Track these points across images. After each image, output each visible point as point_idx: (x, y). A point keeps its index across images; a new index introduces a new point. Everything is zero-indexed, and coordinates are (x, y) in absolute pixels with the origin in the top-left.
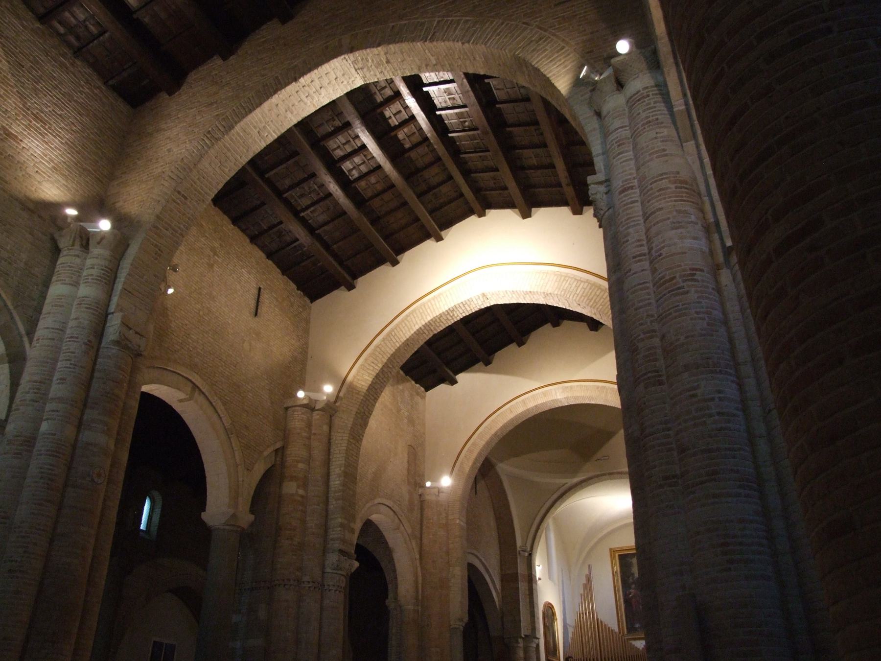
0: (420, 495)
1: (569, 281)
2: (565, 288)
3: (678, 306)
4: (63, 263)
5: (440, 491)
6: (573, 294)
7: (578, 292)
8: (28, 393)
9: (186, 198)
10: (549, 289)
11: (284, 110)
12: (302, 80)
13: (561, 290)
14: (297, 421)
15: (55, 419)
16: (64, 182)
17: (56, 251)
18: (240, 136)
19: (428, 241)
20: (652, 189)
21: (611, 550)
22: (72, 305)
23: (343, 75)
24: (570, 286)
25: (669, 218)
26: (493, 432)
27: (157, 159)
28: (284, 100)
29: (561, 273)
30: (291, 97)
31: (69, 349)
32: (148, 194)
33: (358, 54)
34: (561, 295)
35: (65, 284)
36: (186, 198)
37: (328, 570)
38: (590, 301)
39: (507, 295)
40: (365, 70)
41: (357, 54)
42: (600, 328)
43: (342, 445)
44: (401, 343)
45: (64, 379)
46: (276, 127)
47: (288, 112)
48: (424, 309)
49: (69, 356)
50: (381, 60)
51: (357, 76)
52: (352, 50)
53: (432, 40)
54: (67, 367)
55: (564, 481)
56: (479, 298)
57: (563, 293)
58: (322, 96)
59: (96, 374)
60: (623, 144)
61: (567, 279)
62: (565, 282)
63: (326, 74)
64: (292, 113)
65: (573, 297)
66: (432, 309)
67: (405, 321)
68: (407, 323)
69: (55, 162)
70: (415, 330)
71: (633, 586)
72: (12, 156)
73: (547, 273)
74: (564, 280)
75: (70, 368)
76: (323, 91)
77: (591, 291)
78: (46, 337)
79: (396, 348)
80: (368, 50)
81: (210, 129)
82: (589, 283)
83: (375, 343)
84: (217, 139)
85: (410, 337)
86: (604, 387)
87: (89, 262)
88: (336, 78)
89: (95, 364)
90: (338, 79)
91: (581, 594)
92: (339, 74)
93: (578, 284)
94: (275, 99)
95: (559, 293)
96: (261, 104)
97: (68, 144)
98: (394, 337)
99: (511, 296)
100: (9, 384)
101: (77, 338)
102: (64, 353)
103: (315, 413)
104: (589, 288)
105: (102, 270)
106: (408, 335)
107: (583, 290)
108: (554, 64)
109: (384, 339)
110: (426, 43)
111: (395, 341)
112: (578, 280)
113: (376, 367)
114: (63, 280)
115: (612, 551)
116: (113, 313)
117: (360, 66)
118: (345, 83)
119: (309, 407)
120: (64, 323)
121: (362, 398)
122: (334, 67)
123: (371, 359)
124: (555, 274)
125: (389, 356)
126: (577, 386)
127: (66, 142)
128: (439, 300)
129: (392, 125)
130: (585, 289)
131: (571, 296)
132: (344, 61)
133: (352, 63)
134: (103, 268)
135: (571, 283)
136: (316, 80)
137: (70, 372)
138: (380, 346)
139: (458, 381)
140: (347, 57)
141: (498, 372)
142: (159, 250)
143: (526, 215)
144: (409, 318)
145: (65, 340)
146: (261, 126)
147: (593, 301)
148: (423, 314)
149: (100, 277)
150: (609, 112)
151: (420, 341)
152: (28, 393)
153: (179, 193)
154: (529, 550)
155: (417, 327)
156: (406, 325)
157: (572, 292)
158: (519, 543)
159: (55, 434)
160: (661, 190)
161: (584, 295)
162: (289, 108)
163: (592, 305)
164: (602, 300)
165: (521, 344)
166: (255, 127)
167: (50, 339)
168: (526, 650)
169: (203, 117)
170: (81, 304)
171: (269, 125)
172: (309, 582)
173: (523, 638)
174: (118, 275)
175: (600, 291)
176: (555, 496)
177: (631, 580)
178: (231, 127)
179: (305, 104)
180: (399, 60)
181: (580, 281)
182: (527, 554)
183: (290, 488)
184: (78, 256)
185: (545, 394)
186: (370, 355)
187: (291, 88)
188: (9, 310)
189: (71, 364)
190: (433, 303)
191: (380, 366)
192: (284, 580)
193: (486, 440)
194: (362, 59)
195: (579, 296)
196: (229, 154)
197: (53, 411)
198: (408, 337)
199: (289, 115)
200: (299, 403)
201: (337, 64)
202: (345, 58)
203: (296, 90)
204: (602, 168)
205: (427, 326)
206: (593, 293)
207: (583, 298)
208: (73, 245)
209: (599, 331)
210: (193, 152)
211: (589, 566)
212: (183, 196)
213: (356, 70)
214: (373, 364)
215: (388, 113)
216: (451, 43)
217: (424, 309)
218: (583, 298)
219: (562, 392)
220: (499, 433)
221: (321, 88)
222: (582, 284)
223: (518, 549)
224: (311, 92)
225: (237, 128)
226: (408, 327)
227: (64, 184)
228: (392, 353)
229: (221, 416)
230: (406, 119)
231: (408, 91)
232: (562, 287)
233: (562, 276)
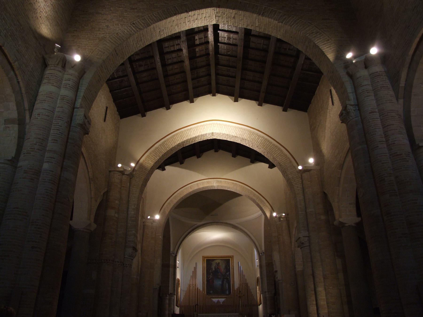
0: (143, 222)
1: (254, 135)
2: (253, 138)
3: (405, 166)
4: (52, 74)
5: (154, 221)
6: (256, 141)
7: (258, 141)
8: (36, 144)
9: (117, 55)
10: (245, 137)
11: (175, 25)
12: (190, 13)
13: (251, 138)
14: (116, 178)
15: (52, 163)
16: (50, 27)
17: (45, 65)
18: (151, 31)
19: (186, 101)
20: (388, 115)
21: (203, 257)
22: (58, 99)
23: (209, 17)
24: (255, 138)
25: (397, 129)
26: (182, 196)
27: (99, 29)
28: (177, 20)
29: (251, 131)
30: (182, 19)
31: (58, 123)
32: (96, 47)
33: (221, 10)
34: (250, 141)
35: (53, 86)
36: (117, 55)
37: (126, 256)
38: (264, 147)
39: (223, 136)
40: (220, 18)
41: (221, 9)
42: (236, 157)
43: (136, 194)
44: (169, 149)
45: (56, 140)
46: (168, 31)
47: (177, 26)
48: (182, 134)
49: (58, 128)
50: (231, 16)
51: (215, 19)
52: (219, 7)
53: (263, 15)
54: (58, 134)
55: (195, 223)
56: (210, 135)
57: (251, 140)
58: (195, 23)
59: (69, 140)
60: (369, 92)
61: (254, 134)
62: (253, 135)
63: (202, 14)
64: (178, 27)
65: (256, 143)
66: (186, 135)
67: (172, 138)
68: (173, 139)
69: (48, 14)
70: (177, 143)
71: (211, 274)
72: (32, 4)
73: (245, 129)
74: (252, 134)
75: (59, 135)
76: (196, 21)
77: (264, 142)
78: (44, 114)
79: (167, 150)
80: (228, 10)
81: (134, 22)
82: (264, 138)
83: (156, 146)
84: (140, 29)
85: (174, 146)
86: (236, 184)
87: (66, 76)
88: (205, 17)
89: (68, 135)
90: (206, 18)
91: (191, 276)
92: (207, 15)
93: (259, 138)
94: (174, 18)
95: (250, 140)
96: (167, 18)
97: (53, 5)
98: (166, 145)
99: (225, 136)
100: (17, 137)
101: (62, 118)
102: (55, 125)
103: (124, 176)
104: (263, 140)
105: (74, 83)
106: (174, 145)
107: (261, 141)
108: (326, 46)
109: (160, 145)
110: (259, 16)
111: (166, 147)
112: (259, 136)
113: (156, 158)
114: (52, 83)
115: (204, 257)
116: (78, 108)
117: (219, 15)
118: (208, 21)
119: (122, 172)
120: (54, 108)
121: (147, 172)
122: (207, 12)
123: (153, 153)
124: (248, 130)
125: (163, 154)
126: (224, 181)
127: (52, 4)
128: (191, 131)
129: (196, 44)
130: (262, 140)
131: (255, 143)
132: (213, 10)
133: (216, 13)
134: (74, 82)
135: (256, 136)
136: (196, 15)
137: (59, 137)
138: (158, 148)
139: (166, 169)
140: (215, 9)
141: (186, 168)
142: (100, 79)
143: (236, 100)
144: (174, 137)
145: (54, 118)
146: (162, 29)
147: (265, 147)
148: (182, 137)
149: (73, 86)
150: (361, 77)
151: (177, 149)
152: (36, 144)
153: (116, 51)
154: (175, 253)
155: (178, 142)
156: (173, 140)
157: (256, 141)
158: (172, 250)
159: (53, 171)
160: (392, 117)
161: (261, 143)
162: (178, 24)
163: (265, 148)
164: (269, 147)
165: (199, 157)
166: (159, 28)
167: (47, 116)
168: (170, 300)
169: (128, 14)
170: (64, 99)
171: (165, 30)
172: (118, 262)
173: (169, 294)
174: (79, 87)
175: (268, 143)
176: (191, 229)
177: (211, 271)
178: (149, 25)
179: (186, 25)
180: (240, 19)
181: (259, 136)
182: (174, 255)
183: (111, 213)
184: (60, 72)
185: (208, 182)
186: (153, 151)
187: (183, 15)
188: (22, 93)
189: (60, 132)
190: (187, 132)
191: (158, 158)
192: (107, 260)
193: (177, 200)
194: (222, 13)
195: (259, 143)
196: (142, 38)
197: (51, 158)
198: (173, 146)
199: (176, 27)
200: (117, 169)
201: (209, 11)
202: (214, 9)
203: (185, 17)
204: (352, 99)
205: (183, 142)
206: (266, 143)
207: (261, 144)
208: (58, 65)
209: (236, 158)
210: (125, 31)
211: (196, 263)
212: (117, 53)
213: (216, 16)
214: (154, 156)
215: (197, 37)
216: (272, 20)
217: (182, 134)
218: (261, 144)
219: (216, 183)
220: (183, 198)
221: (196, 19)
222: (261, 138)
223: (171, 252)
224: (191, 20)
225: (152, 26)
226: (173, 141)
227: (49, 28)
228: (165, 152)
229: (89, 171)
230: (203, 43)
231: (212, 30)
232: (251, 137)
233: (251, 132)
